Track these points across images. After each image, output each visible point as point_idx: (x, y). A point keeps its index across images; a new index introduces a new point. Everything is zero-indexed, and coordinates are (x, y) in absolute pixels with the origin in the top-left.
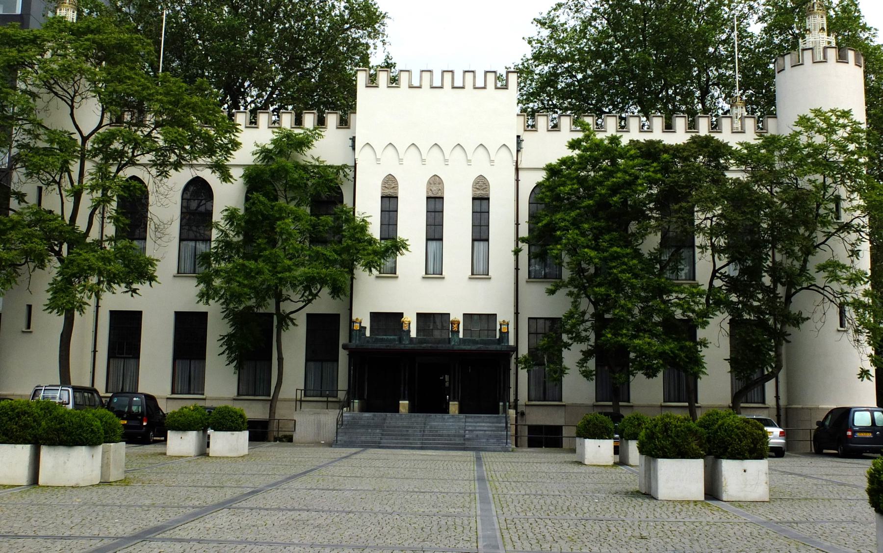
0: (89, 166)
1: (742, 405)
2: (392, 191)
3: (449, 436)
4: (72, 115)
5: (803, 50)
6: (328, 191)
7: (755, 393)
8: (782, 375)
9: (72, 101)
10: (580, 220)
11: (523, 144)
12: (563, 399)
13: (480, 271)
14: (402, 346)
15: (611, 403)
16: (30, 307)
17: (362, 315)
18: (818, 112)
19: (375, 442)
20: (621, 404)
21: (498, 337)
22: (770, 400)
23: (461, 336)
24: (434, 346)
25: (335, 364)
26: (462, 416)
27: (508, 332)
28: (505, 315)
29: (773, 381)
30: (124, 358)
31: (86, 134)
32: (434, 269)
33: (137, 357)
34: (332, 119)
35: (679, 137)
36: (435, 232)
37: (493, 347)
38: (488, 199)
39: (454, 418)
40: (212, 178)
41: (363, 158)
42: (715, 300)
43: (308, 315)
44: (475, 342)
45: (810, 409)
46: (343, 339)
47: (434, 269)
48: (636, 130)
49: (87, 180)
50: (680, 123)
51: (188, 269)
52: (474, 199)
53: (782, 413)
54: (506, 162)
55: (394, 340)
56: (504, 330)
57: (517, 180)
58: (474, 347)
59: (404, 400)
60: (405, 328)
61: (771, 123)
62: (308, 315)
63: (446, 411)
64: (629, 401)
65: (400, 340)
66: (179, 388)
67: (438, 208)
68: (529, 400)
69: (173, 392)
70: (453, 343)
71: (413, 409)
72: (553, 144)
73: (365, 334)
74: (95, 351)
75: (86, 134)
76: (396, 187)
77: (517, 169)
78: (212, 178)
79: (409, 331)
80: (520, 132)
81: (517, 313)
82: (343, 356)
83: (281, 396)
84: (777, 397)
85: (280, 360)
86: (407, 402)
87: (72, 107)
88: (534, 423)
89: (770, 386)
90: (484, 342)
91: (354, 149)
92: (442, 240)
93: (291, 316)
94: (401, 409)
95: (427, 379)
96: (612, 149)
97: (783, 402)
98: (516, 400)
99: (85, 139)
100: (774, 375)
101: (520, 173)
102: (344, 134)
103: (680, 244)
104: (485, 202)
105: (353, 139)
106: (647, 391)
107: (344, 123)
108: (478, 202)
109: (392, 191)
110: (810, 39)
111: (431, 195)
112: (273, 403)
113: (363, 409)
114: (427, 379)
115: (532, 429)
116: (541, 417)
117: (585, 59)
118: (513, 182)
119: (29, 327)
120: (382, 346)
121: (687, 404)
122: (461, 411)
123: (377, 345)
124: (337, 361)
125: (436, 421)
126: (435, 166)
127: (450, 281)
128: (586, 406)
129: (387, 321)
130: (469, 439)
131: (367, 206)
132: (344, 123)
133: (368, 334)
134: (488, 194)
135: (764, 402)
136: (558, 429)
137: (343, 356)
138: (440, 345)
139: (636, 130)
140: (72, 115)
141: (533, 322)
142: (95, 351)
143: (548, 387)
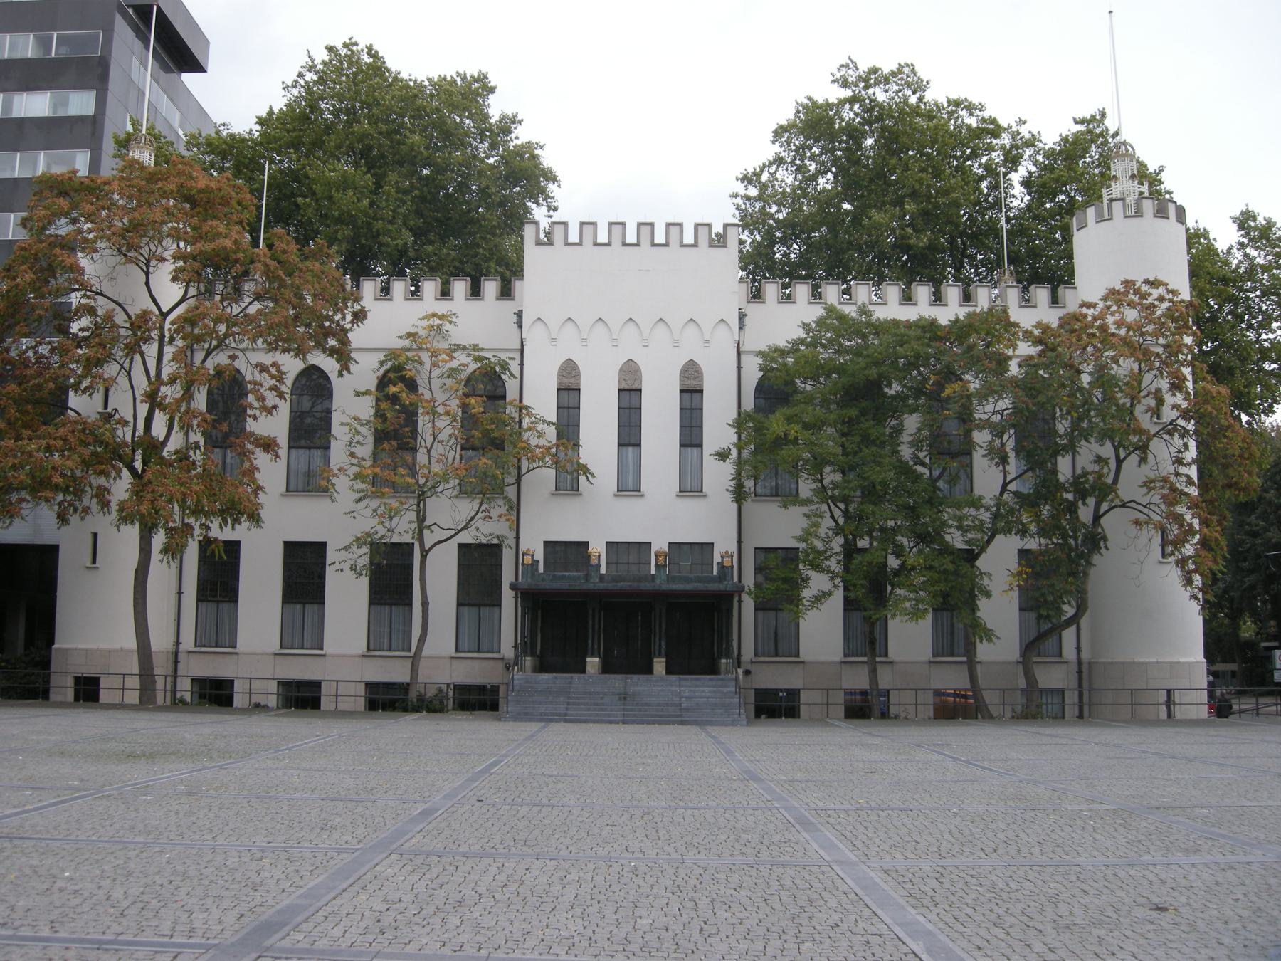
0: (169, 351)
1: (1036, 659)
2: (572, 381)
3: (659, 705)
4: (147, 284)
5: (1112, 200)
6: (489, 383)
7: (1051, 642)
8: (1084, 621)
9: (148, 265)
10: (817, 419)
11: (747, 320)
12: (890, 654)
13: (691, 486)
14: (591, 586)
15: (865, 659)
16: (95, 535)
17: (533, 544)
18: (1128, 283)
19: (559, 714)
20: (878, 659)
21: (653, 572)
22: (1069, 652)
23: (603, 570)
24: (635, 584)
25: (496, 609)
26: (674, 677)
27: (732, 567)
28: (724, 544)
29: (1073, 629)
30: (218, 602)
31: (165, 310)
32: (629, 484)
33: (234, 599)
34: (490, 287)
35: (950, 311)
36: (630, 433)
37: (713, 587)
38: (701, 391)
39: (659, 682)
40: (329, 365)
41: (534, 336)
42: (1004, 521)
43: (460, 545)
44: (621, 579)
45: (1123, 663)
46: (507, 576)
47: (629, 484)
48: (889, 305)
49: (166, 371)
50: (953, 293)
51: (301, 486)
52: (681, 391)
53: (1085, 668)
54: (725, 342)
55: (579, 578)
56: (727, 562)
57: (739, 368)
58: (689, 587)
59: (593, 655)
60: (594, 561)
61: (1065, 293)
62: (460, 545)
63: (649, 670)
64: (886, 655)
65: (587, 577)
66: (465, 643)
67: (634, 403)
68: (756, 655)
69: (457, 650)
70: (658, 582)
71: (607, 668)
72: (788, 319)
73: (537, 570)
74: (180, 593)
75: (165, 310)
76: (577, 376)
77: (739, 353)
78: (329, 365)
79: (599, 566)
80: (744, 305)
81: (739, 542)
82: (508, 597)
83: (425, 652)
84: (1078, 649)
85: (425, 604)
86: (597, 659)
87: (147, 274)
88: (763, 686)
89: (1069, 635)
90: (699, 580)
91: (521, 327)
92: (639, 445)
93: (1079, 472)
94: (588, 668)
95: (623, 630)
96: (866, 327)
97: (1085, 655)
98: (739, 655)
99: (164, 315)
100: (1075, 620)
101: (743, 357)
102: (508, 307)
103: (952, 451)
104: (696, 395)
105: (519, 314)
106: (910, 637)
107: (506, 292)
108: (686, 396)
109: (572, 381)
110: (1117, 189)
111: (624, 386)
112: (415, 659)
113: (542, 668)
114: (623, 630)
115: (761, 694)
116: (775, 677)
117: (792, 229)
118: (735, 370)
119: (94, 561)
120: (564, 585)
121: (964, 659)
122: (669, 672)
123: (556, 585)
124: (411, 604)
125: (637, 683)
126: (631, 349)
127: (654, 507)
128: (1009, 663)
129: (568, 553)
130: (687, 709)
131: (541, 398)
132: (506, 292)
133: (541, 570)
134: (701, 385)
135: (1060, 655)
136: (794, 694)
137: (508, 597)
138: (621, 584)
139: (889, 305)
140: (147, 284)
141: (762, 555)
142: (180, 593)
143: (781, 642)
